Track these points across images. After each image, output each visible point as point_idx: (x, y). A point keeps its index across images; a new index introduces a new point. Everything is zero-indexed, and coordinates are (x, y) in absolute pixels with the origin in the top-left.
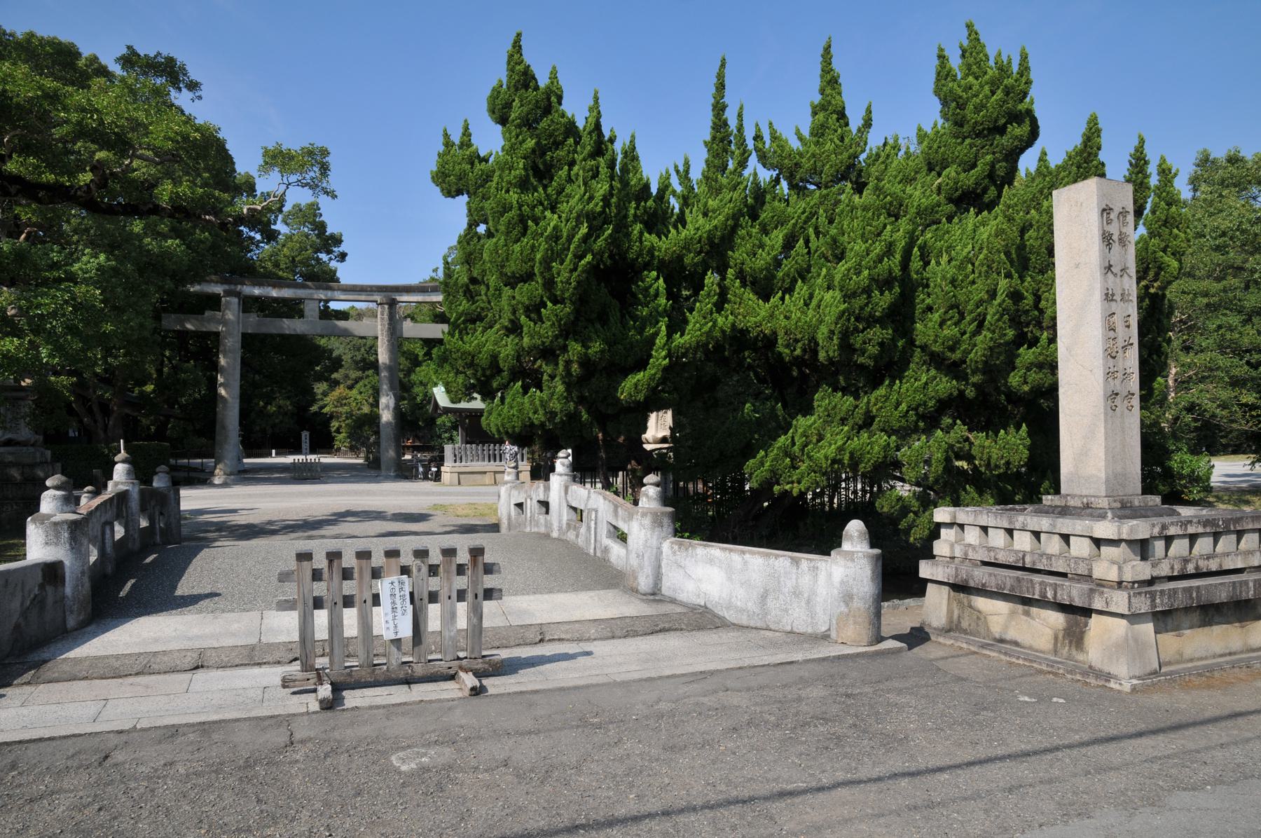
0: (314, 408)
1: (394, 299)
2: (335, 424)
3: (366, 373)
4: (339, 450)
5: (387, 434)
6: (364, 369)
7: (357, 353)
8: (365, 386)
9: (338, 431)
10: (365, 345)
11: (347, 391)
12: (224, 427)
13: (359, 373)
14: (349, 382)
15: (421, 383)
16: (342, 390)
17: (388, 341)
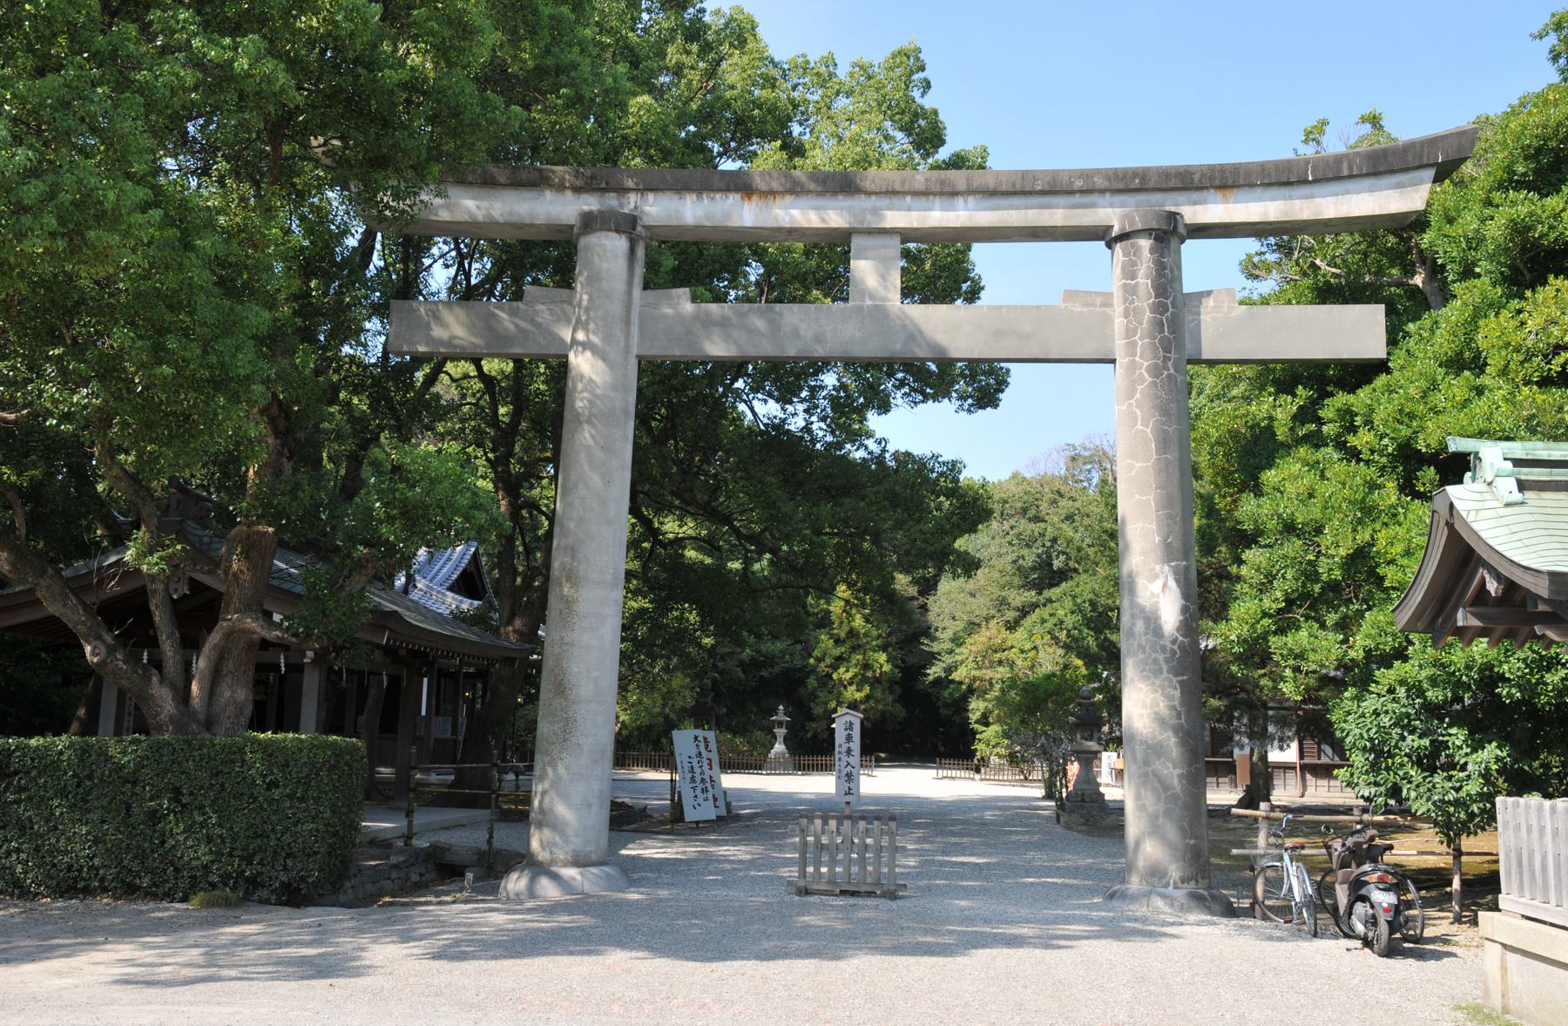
0: (935, 671)
1: (1173, 217)
2: (976, 707)
3: (1047, 593)
4: (984, 761)
5: (312, 684)
6: (1039, 587)
7: (1025, 552)
8: (1043, 621)
9: (985, 721)
10: (1042, 535)
11: (1005, 634)
12: (561, 689)
13: (1031, 596)
14: (1011, 615)
15: (1289, 528)
16: (994, 631)
17: (1156, 371)
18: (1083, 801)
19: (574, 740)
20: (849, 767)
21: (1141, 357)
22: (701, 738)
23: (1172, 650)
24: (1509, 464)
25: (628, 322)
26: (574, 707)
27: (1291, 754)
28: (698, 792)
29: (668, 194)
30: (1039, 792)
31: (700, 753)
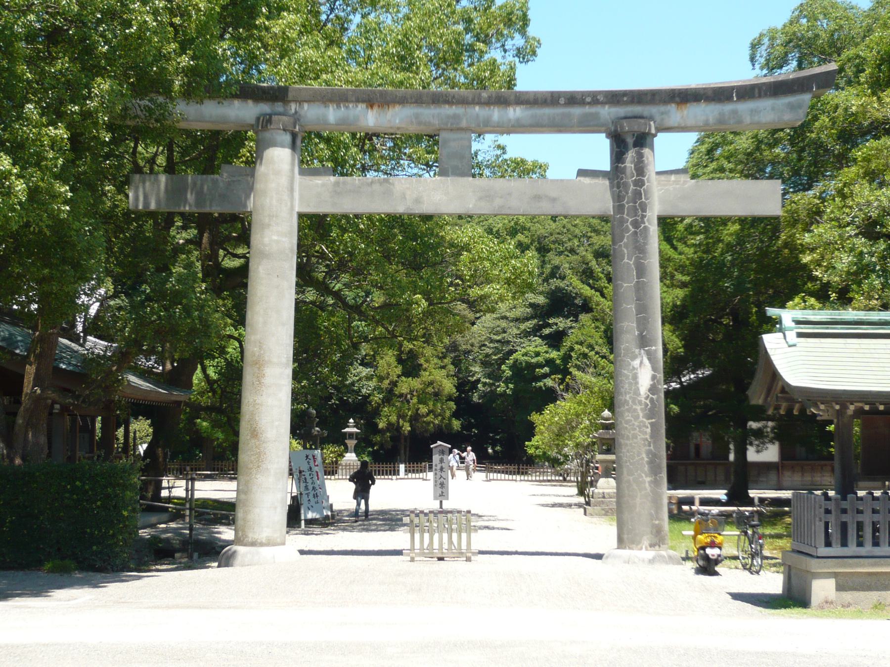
12: (255, 434)
18: (604, 497)
19: (264, 466)
20: (442, 479)
21: (627, 215)
22: (311, 457)
23: (645, 403)
24: (793, 323)
25: (292, 190)
26: (264, 445)
27: (771, 453)
28: (311, 497)
29: (317, 103)
30: (575, 491)
31: (311, 468)
